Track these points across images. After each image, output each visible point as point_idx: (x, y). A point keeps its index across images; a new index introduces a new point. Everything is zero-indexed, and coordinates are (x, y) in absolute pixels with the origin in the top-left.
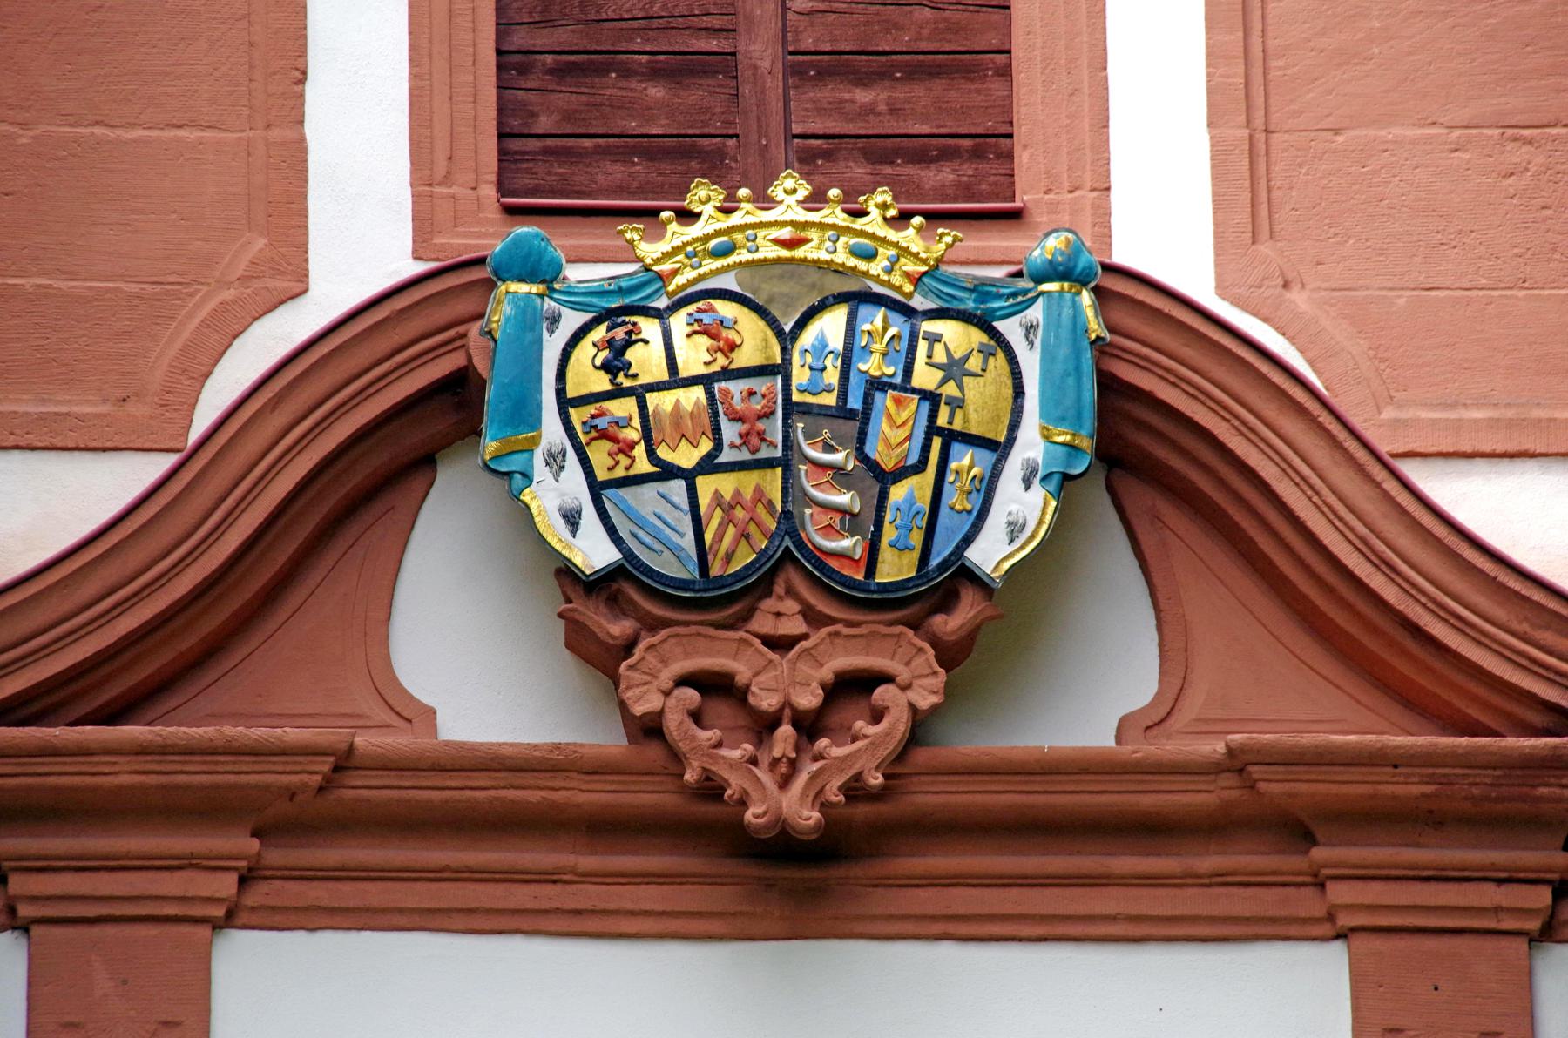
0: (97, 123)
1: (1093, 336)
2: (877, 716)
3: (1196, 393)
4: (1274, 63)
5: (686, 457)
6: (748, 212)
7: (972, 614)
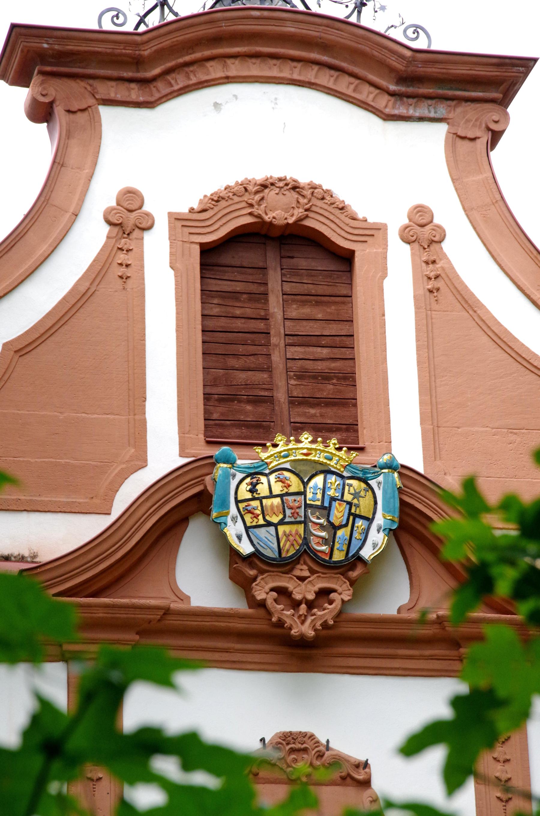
0: (83, 413)
1: (398, 486)
2: (331, 602)
3: (427, 506)
4: (439, 406)
5: (275, 519)
6: (293, 445)
7: (360, 572)
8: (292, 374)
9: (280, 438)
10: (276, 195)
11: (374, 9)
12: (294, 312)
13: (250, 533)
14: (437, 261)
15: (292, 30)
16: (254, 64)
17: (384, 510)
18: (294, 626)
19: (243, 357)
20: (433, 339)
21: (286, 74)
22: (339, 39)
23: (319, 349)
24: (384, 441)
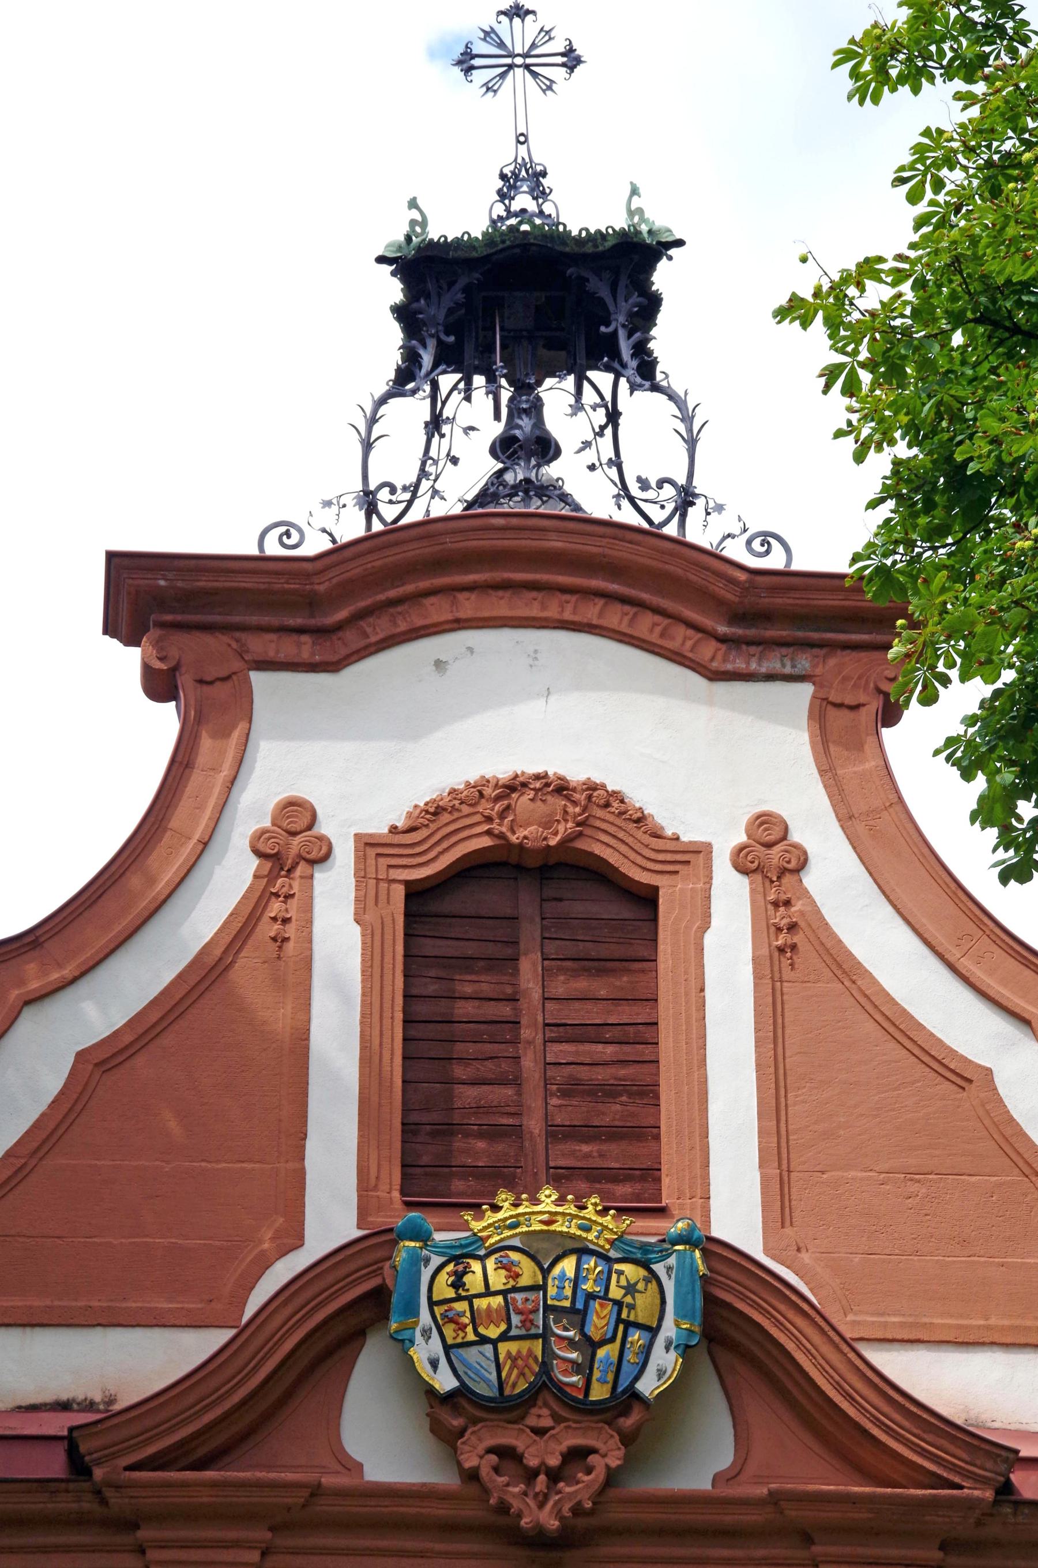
0: (203, 1161)
1: (701, 1273)
2: (589, 1471)
4: (791, 1137)
8: (555, 1087)
9: (503, 1196)
10: (529, 802)
11: (706, 510)
12: (560, 987)
13: (453, 1358)
14: (793, 902)
15: (559, 544)
16: (502, 598)
17: (676, 1313)
18: (526, 1512)
19: (474, 1063)
20: (783, 1027)
21: (552, 612)
22: (634, 557)
23: (600, 1047)
24: (699, 1196)
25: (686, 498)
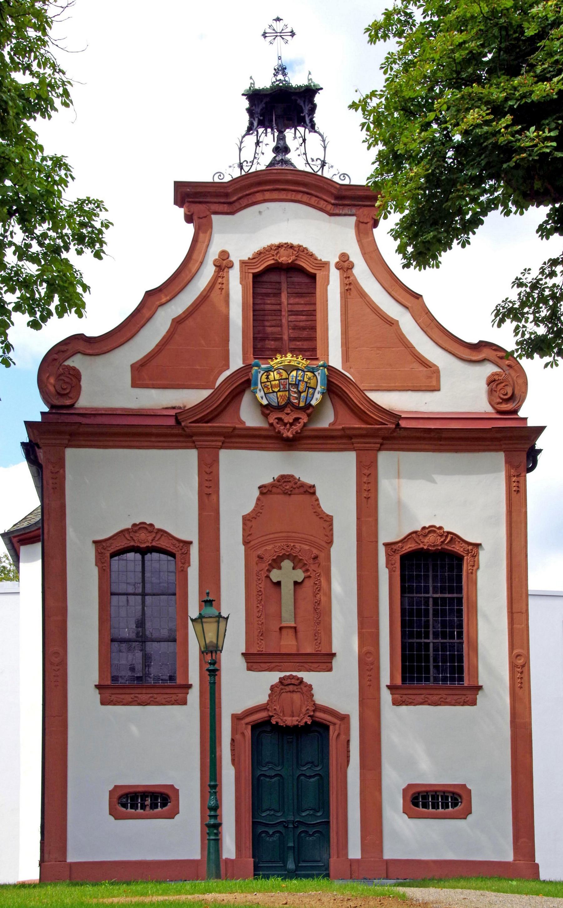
2: (299, 423)
5: (276, 390)
12: (292, 301)
17: (321, 384)
23: (302, 317)
25: (323, 164)
